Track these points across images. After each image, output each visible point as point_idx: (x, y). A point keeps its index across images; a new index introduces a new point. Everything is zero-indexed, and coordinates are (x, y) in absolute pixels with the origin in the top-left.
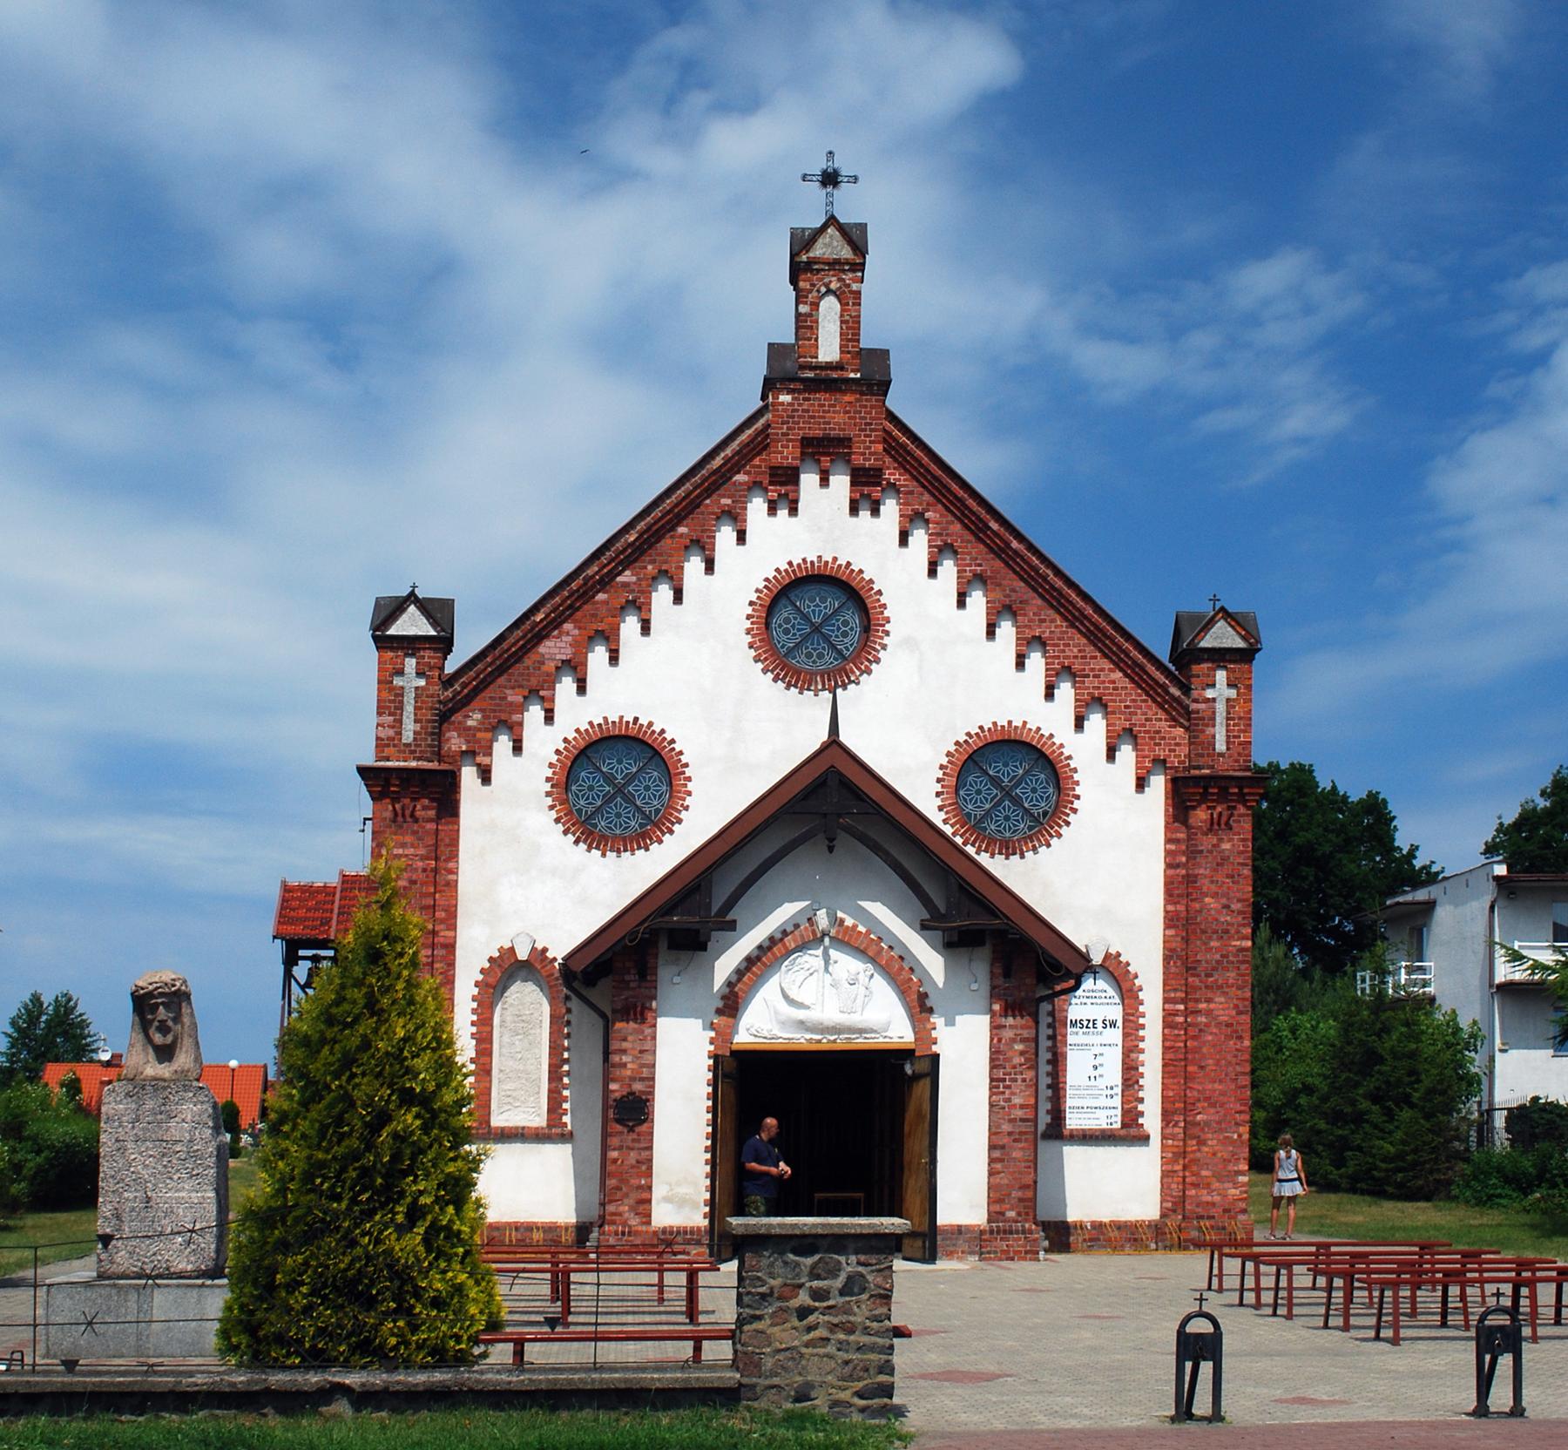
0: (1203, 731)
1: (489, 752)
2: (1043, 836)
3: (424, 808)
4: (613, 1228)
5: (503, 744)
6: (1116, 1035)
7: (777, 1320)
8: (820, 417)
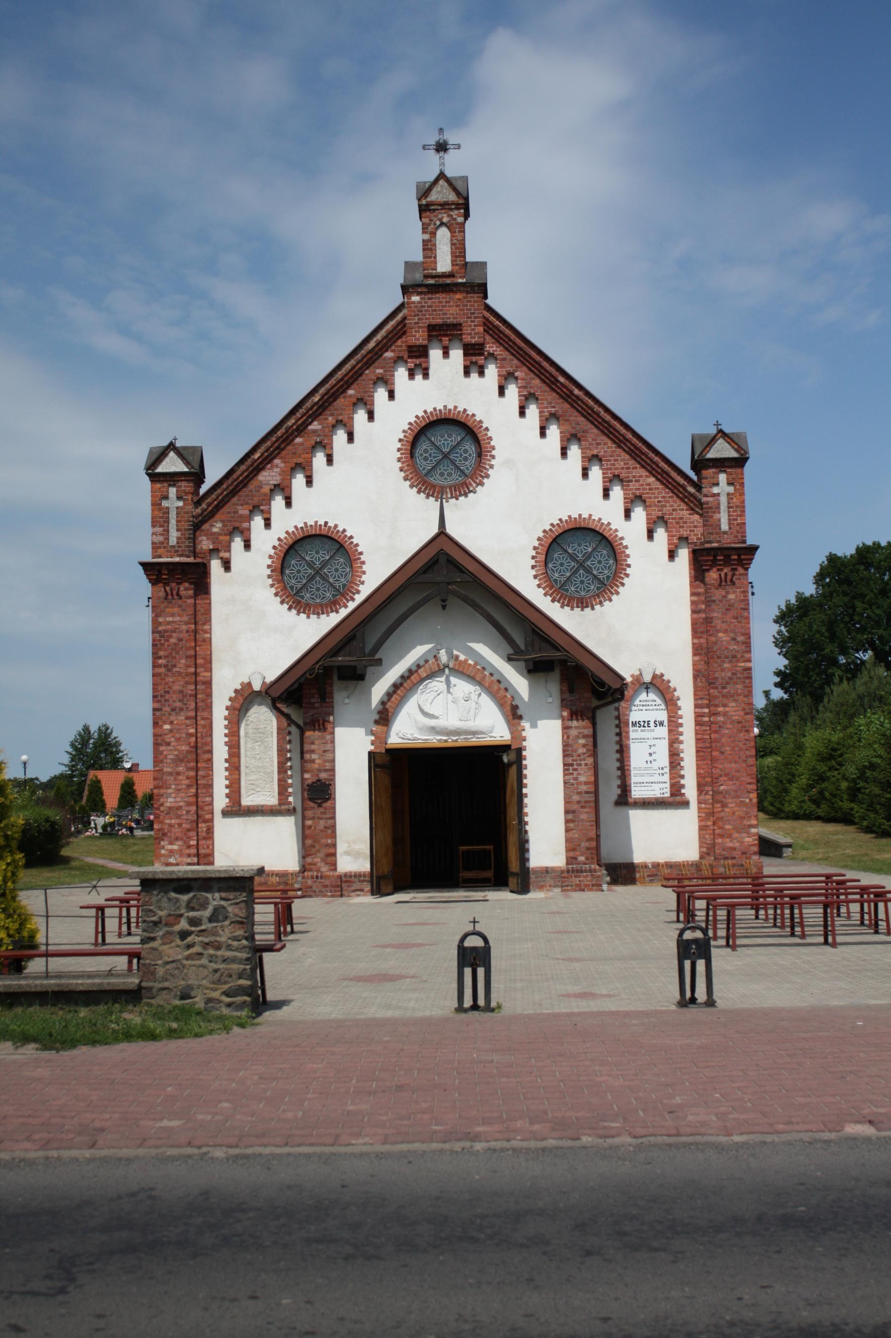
0: (712, 517)
1: (228, 549)
2: (606, 593)
3: (186, 589)
4: (310, 874)
5: (237, 543)
6: (663, 731)
7: (166, 940)
8: (440, 310)
